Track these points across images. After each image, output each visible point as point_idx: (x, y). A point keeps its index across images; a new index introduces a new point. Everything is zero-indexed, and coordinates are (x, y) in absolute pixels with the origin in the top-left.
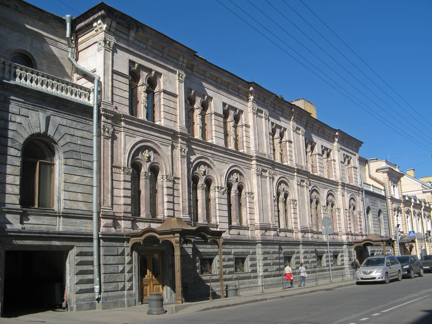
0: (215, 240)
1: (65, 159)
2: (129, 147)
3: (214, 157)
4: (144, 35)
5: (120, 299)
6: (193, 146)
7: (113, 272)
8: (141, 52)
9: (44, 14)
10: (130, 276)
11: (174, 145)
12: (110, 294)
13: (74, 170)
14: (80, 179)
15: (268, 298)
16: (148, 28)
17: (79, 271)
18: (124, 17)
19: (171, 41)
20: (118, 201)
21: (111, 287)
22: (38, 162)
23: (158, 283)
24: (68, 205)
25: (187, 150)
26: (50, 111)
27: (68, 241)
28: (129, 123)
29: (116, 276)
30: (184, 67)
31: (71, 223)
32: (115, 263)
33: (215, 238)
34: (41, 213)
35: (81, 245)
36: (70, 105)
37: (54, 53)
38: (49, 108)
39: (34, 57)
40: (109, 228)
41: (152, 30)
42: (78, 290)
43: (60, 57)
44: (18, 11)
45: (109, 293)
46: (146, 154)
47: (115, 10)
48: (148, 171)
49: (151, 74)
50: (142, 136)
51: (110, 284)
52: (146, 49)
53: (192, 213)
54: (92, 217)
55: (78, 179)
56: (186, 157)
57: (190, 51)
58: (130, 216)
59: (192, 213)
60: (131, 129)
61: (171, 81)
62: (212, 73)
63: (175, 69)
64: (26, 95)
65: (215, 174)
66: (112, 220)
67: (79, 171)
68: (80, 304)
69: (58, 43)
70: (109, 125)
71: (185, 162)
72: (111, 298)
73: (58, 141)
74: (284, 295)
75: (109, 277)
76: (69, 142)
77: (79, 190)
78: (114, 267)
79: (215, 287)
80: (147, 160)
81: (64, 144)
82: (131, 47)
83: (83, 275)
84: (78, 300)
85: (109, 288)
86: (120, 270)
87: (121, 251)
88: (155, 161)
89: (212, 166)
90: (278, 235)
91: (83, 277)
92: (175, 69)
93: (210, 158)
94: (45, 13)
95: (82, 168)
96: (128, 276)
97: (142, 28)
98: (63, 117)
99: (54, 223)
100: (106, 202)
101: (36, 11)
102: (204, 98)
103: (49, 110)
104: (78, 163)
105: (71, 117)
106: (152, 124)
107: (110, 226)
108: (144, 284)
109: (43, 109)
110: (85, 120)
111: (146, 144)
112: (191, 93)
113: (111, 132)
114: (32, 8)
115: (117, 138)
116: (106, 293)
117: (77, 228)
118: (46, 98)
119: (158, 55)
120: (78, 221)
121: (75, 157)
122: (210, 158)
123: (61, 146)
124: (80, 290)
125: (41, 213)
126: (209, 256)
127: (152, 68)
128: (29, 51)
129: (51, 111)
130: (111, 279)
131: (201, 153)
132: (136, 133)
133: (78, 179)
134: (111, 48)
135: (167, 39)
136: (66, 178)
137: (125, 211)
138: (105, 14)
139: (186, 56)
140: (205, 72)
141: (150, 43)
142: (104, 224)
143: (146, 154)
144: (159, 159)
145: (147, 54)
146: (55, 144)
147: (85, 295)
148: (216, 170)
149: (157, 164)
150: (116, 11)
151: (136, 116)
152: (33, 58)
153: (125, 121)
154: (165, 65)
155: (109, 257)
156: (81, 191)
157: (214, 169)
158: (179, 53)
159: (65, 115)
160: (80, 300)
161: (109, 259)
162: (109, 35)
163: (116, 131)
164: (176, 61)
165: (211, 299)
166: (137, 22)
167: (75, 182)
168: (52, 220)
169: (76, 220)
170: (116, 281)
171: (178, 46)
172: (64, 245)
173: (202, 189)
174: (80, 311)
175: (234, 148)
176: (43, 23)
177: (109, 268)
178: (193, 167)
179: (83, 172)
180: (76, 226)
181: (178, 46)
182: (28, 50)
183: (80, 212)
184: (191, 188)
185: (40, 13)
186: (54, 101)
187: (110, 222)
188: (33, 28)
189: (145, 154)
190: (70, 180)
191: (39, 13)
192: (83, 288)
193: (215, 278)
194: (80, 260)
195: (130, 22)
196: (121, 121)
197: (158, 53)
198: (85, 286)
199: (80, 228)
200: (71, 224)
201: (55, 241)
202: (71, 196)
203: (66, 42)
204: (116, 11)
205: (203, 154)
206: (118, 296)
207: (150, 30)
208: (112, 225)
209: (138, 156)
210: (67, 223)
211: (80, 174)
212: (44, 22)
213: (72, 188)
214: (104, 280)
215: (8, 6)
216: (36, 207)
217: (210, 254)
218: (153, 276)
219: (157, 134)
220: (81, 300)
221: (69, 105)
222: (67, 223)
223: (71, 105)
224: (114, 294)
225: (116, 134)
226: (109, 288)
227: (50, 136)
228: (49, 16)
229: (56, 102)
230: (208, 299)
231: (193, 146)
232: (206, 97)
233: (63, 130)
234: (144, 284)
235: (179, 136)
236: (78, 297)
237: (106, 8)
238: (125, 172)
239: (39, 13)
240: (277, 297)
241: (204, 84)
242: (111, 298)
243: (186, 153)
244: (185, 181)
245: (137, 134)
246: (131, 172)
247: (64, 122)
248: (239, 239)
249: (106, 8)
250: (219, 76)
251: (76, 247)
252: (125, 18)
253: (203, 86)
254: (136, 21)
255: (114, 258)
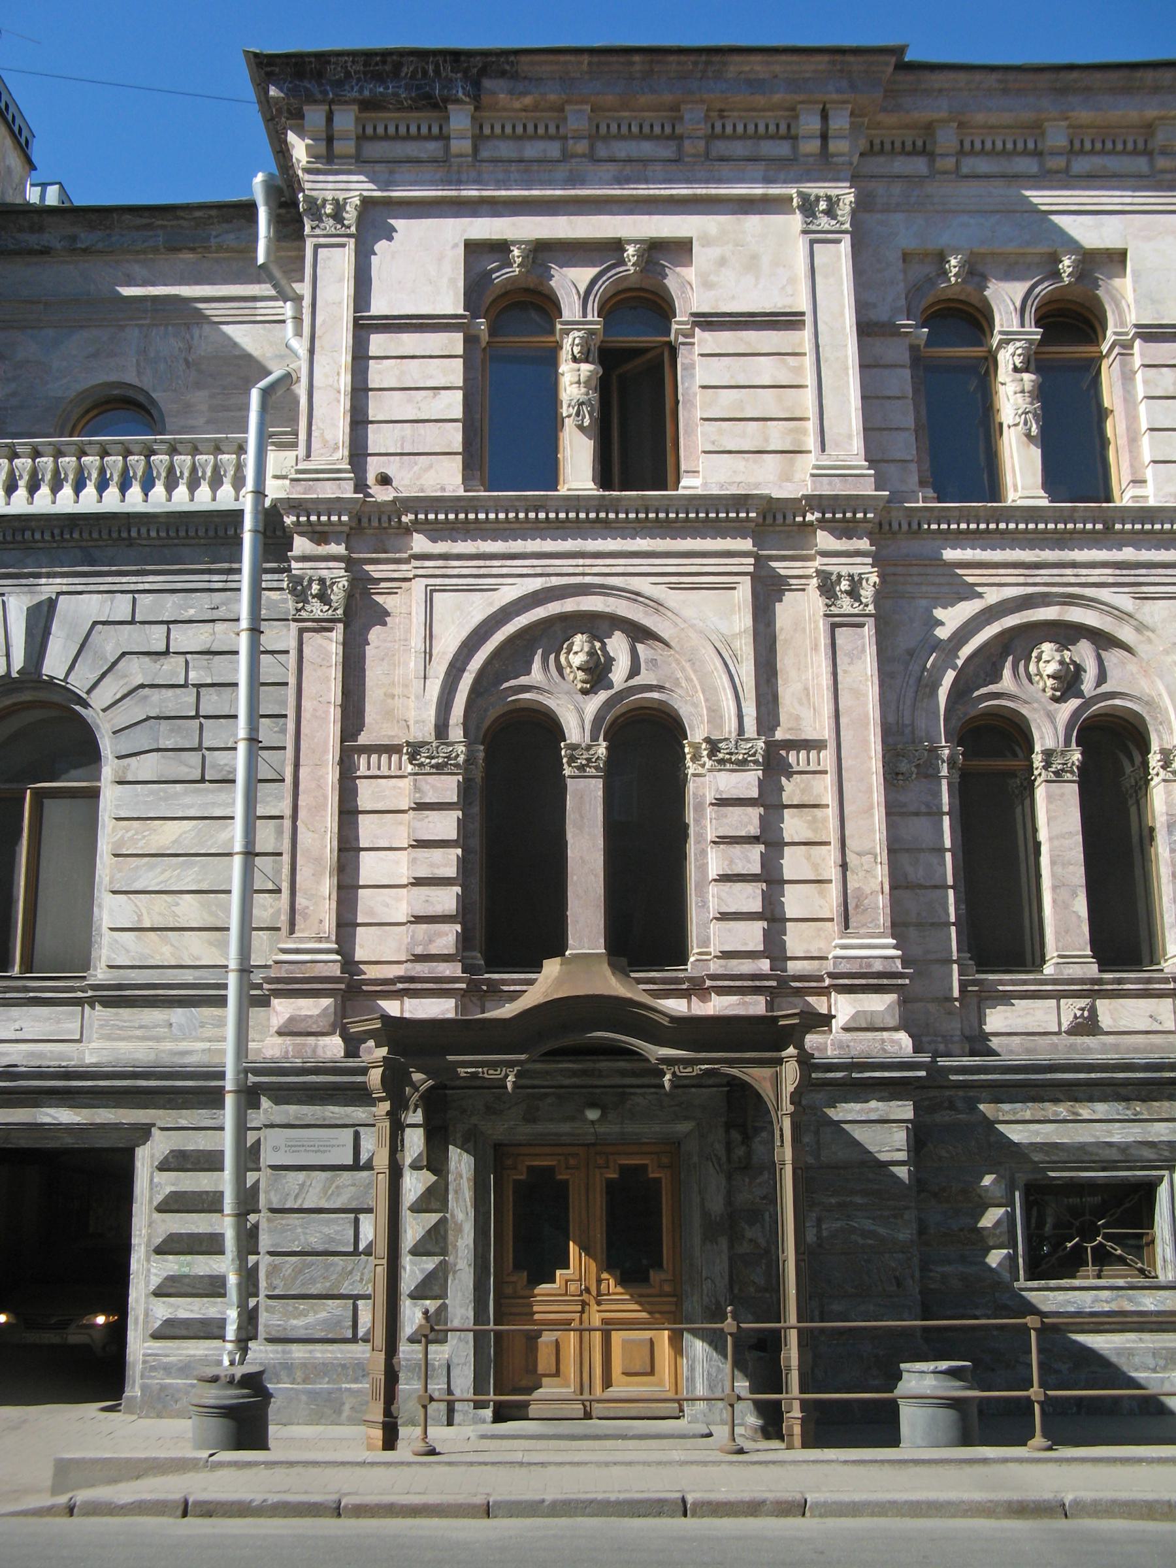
0: (734, 1071)
1: (118, 758)
2: (448, 643)
3: (1141, 579)
4: (528, 100)
5: (356, 1381)
6: (950, 554)
7: (320, 1248)
8: (529, 185)
9: (178, 218)
10: (422, 1270)
11: (782, 572)
12: (298, 1352)
13: (161, 799)
14: (193, 834)
15: (816, 1504)
16: (537, 58)
17: (164, 1236)
18: (384, 62)
19: (704, 58)
20: (387, 906)
21: (310, 1319)
22: (28, 791)
23: (644, 1315)
24: (128, 951)
25: (874, 578)
26: (51, 581)
27: (117, 1106)
28: (453, 529)
29: (340, 1268)
30: (840, 160)
31: (141, 1027)
32: (337, 1205)
33: (731, 1062)
34: (8, 995)
35: (183, 1123)
36: (139, 531)
37: (243, 350)
38: (44, 570)
39: (154, 395)
40: (311, 1040)
41: (562, 58)
42: (159, 1323)
43: (268, 355)
44: (86, 251)
45: (294, 1347)
46: (576, 653)
47: (322, 58)
48: (588, 740)
49: (622, 262)
50: (539, 570)
51: (302, 1305)
52: (566, 157)
53: (949, 924)
54: (222, 992)
55: (180, 836)
56: (871, 622)
57: (851, 58)
58: (447, 973)
59: (949, 924)
60: (459, 557)
61: (755, 257)
62: (1084, 115)
63: (775, 190)
64: (41, 545)
65: (1161, 677)
66: (891, 998)
67: (188, 800)
68: (163, 1388)
69: (259, 304)
70: (331, 564)
71: (863, 651)
72: (299, 1375)
73: (89, 692)
74: (1068, 1498)
75: (298, 1271)
76: (142, 686)
77: (187, 880)
78: (328, 1223)
79: (1151, 1362)
80: (584, 682)
81: (118, 696)
82: (467, 182)
83: (189, 1257)
84: (153, 1368)
85: (294, 1322)
86: (367, 1238)
87: (370, 1147)
88: (644, 678)
89: (1125, 633)
90: (1088, 1025)
91: (188, 1264)
92: (775, 190)
93: (1104, 594)
94: (181, 213)
95: (207, 784)
96: (412, 1271)
97: (503, 74)
98: (115, 588)
99: (72, 1032)
100: (306, 917)
101: (145, 221)
102: (1056, 275)
103: (49, 575)
104: (186, 765)
105: (151, 578)
106: (595, 503)
107: (314, 1029)
108: (537, 1317)
109: (24, 581)
110: (224, 577)
111: (570, 605)
112: (945, 273)
113: (342, 594)
114: (127, 217)
115: (388, 614)
116: (279, 1347)
117: (168, 1046)
118: (28, 534)
119: (645, 162)
120: (178, 1015)
121: (169, 744)
122: (1104, 594)
123: (104, 710)
124: (169, 1323)
125: (8, 995)
126: (1104, 1169)
127: (619, 236)
128: (135, 381)
129: (58, 581)
130: (313, 1281)
131: (1021, 580)
132: (497, 567)
133: (185, 832)
134: (349, 227)
135: (671, 58)
136: (123, 837)
137: (419, 950)
138: (282, 95)
139: (835, 96)
140: (1037, 128)
141: (577, 120)
142: (282, 1021)
143: (576, 653)
144: (674, 665)
145: (573, 180)
146: (86, 708)
147: (197, 1348)
148: (1167, 652)
149: (655, 695)
150: (333, 60)
151: (1109, 499)
152: (153, 402)
153: (427, 527)
154: (699, 191)
155: (302, 1176)
156: (199, 882)
157: (1141, 649)
158: (777, 98)
159: (124, 579)
160: (165, 1369)
161: (302, 1186)
162: (331, 178)
163: (383, 585)
164: (782, 149)
165: (1038, 1440)
166: (463, 58)
167: (168, 848)
168: (58, 1022)
169: (167, 1011)
170: (342, 1291)
171: (758, 68)
172: (98, 1121)
173: (1052, 777)
174: (159, 1416)
175: (1042, 493)
176: (191, 256)
177: (299, 1230)
178: (954, 668)
179: (210, 798)
180: (165, 1038)
181: (758, 68)
182: (131, 377)
183: (188, 977)
184: (944, 783)
185: (165, 223)
186: (67, 536)
187: (881, 1007)
188: (151, 288)
189: (1041, 664)
190: (141, 843)
191: (160, 222)
192: (183, 1314)
193: (1152, 1308)
194: (173, 1189)
195: (425, 73)
196: (407, 531)
197: (647, 148)
198: (196, 1308)
199: (184, 1046)
200: (139, 1033)
201: (57, 1106)
202: (144, 911)
203: (266, 289)
204: (333, 60)
205: (1037, 580)
206: (344, 1366)
207: (551, 58)
208: (892, 1022)
209: (529, 673)
210: (121, 1028)
211: (191, 813)
212: (193, 250)
213: (151, 874)
214: (271, 1286)
215: (45, 251)
216: (16, 971)
217: (1115, 1155)
218: (605, 1275)
219: (549, 546)
220: (167, 1369)
221: (134, 534)
222: (121, 1028)
223: (144, 531)
224: (319, 1355)
225: (379, 599)
226: (294, 1322)
227: (52, 678)
228: (200, 218)
229: (76, 535)
230: (1021, 1440)
231: (950, 554)
232: (1066, 264)
233: (110, 643)
234: (537, 1317)
235: (809, 517)
236: (156, 1355)
237: (277, 70)
238: (421, 765)
239: (160, 222)
240: (949, 1503)
241: (1040, 198)
242: (299, 1375)
243: (870, 600)
244: (867, 750)
245: (504, 571)
246: (461, 759)
247: (121, 607)
248: (1077, 1058)
249: (277, 70)
250: (1151, 113)
251: (162, 1129)
252: (388, 68)
253: (1034, 210)
254: (455, 56)
255: (332, 1180)
